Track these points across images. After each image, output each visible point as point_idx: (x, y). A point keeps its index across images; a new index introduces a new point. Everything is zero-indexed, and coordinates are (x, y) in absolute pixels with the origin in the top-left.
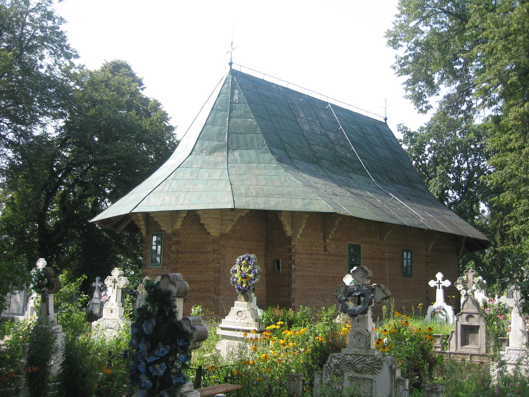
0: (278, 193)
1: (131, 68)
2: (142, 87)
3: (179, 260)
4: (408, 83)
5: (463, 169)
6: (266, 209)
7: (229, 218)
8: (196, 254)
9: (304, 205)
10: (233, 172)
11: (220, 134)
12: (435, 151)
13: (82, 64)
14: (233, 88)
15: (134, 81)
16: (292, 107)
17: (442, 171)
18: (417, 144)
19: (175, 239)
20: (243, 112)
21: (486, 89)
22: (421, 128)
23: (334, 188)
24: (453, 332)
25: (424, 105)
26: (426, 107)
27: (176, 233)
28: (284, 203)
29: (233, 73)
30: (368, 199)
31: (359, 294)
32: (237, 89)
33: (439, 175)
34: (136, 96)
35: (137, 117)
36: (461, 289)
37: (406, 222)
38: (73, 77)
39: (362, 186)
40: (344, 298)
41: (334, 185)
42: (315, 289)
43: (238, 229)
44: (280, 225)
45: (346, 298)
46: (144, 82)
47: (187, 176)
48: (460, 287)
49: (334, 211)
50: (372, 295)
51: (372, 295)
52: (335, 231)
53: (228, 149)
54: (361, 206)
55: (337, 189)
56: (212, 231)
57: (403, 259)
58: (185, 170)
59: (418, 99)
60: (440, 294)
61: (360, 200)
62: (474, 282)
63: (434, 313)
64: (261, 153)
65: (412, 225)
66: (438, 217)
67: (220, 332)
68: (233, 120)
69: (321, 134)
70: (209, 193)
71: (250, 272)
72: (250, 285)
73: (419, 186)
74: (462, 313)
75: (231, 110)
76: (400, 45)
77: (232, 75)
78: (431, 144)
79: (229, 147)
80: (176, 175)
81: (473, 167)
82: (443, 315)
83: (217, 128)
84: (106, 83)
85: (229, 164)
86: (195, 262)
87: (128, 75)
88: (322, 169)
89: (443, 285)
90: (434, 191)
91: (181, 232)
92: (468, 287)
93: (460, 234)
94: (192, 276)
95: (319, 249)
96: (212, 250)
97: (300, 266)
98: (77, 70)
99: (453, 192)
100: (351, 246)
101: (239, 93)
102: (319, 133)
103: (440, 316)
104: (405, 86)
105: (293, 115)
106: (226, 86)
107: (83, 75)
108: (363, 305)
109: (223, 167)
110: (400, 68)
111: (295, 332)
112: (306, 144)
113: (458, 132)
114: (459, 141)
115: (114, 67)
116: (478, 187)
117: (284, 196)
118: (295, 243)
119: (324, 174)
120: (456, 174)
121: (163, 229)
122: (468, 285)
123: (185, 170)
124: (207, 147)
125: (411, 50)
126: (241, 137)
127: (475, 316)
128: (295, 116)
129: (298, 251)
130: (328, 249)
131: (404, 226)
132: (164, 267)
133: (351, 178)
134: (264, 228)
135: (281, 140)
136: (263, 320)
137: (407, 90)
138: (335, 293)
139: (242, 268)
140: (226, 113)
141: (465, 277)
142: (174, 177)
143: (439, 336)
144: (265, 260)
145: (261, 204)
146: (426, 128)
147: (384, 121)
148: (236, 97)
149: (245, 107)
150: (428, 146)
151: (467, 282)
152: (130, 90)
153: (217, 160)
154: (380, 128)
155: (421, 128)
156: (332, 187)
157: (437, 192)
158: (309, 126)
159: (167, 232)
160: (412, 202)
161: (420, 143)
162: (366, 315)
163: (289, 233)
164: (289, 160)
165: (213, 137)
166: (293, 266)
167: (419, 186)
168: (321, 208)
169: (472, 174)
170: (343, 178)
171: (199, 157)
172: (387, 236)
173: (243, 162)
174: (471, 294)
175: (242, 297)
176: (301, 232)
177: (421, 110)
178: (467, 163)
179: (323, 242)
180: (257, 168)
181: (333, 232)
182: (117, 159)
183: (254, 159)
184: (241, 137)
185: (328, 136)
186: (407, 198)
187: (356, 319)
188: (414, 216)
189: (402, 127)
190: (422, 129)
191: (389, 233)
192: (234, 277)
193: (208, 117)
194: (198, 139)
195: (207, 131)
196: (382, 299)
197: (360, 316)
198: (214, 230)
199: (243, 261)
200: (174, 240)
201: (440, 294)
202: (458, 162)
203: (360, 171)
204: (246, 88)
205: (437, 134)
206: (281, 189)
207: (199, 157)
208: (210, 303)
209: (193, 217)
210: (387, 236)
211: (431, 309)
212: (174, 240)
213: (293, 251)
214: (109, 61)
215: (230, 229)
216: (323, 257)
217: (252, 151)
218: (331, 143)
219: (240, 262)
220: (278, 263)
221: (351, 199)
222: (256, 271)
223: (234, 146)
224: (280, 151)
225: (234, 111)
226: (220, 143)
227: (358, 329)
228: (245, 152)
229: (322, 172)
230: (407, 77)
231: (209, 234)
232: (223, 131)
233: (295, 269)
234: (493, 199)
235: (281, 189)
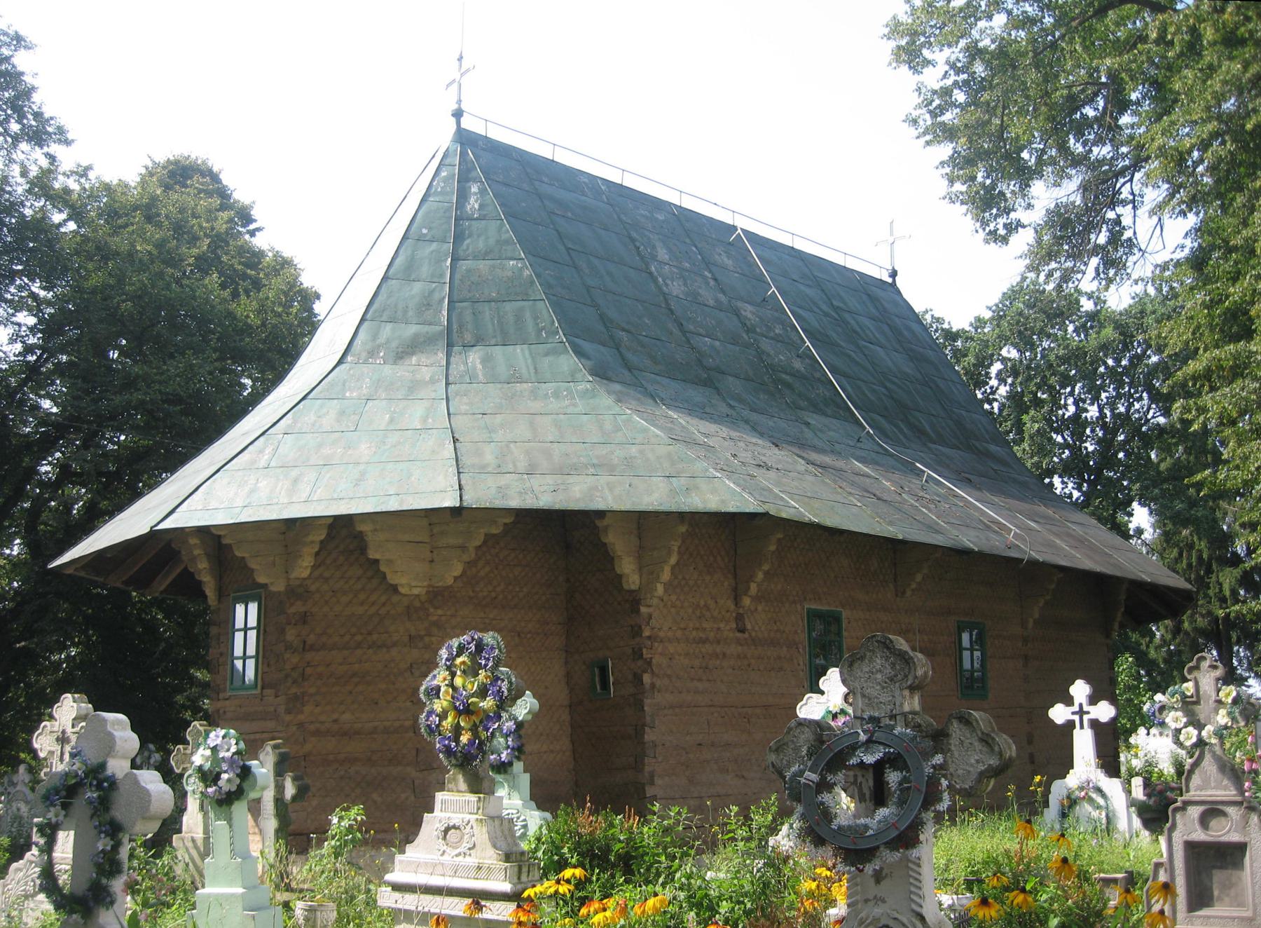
0: (595, 461)
1: (221, 176)
2: (252, 227)
3: (309, 670)
4: (953, 160)
5: (1086, 423)
6: (557, 507)
7: (452, 541)
8: (359, 652)
9: (673, 492)
10: (464, 408)
11: (427, 304)
12: (1016, 377)
13: (85, 164)
14: (464, 178)
15: (223, 207)
16: (634, 235)
17: (1037, 426)
18: (971, 359)
19: (297, 608)
20: (492, 241)
21: (1181, 154)
22: (978, 319)
23: (759, 449)
24: (1158, 866)
25: (1001, 221)
26: (1005, 225)
27: (296, 592)
28: (611, 490)
29: (464, 138)
30: (857, 479)
31: (879, 755)
32: (476, 180)
33: (1031, 437)
34: (227, 244)
35: (226, 294)
36: (1180, 725)
37: (969, 540)
38: (61, 199)
39: (837, 447)
40: (814, 777)
41: (760, 442)
42: (713, 745)
43: (482, 573)
44: (606, 558)
45: (823, 778)
46: (255, 213)
47: (328, 422)
48: (1176, 720)
49: (760, 510)
50: (938, 759)
51: (938, 759)
52: (767, 573)
53: (450, 345)
54: (839, 498)
55: (769, 453)
56: (404, 581)
57: (961, 649)
58: (321, 407)
59: (986, 203)
60: (1084, 744)
61: (834, 481)
62: (1219, 702)
63: (1071, 802)
64: (547, 354)
66: (1054, 529)
67: (387, 899)
68: (464, 265)
69: (719, 307)
70: (390, 466)
71: (483, 692)
72: (483, 735)
73: (993, 448)
74: (1187, 804)
75: (459, 238)
76: (928, 62)
77: (462, 144)
78: (1004, 360)
79: (453, 340)
80: (295, 421)
81: (1114, 415)
82: (1099, 807)
83: (417, 288)
84: (149, 210)
85: (451, 387)
86: (354, 675)
87: (209, 194)
88: (724, 399)
89: (1092, 716)
91: (313, 588)
92: (1202, 717)
93: (1118, 574)
94: (347, 716)
95: (722, 625)
96: (406, 639)
97: (669, 677)
98: (72, 179)
99: (1063, 482)
100: (814, 615)
101: (482, 192)
102: (711, 303)
103: (1088, 807)
104: (947, 170)
105: (639, 254)
106: (444, 174)
107: (93, 196)
108: (901, 803)
109: (433, 395)
110: (929, 122)
111: (624, 910)
112: (676, 331)
113: (1071, 328)
114: (1078, 348)
115: (172, 174)
116: (1127, 466)
117: (611, 469)
118: (651, 610)
119: (730, 412)
120: (1072, 435)
121: (261, 579)
122: (1202, 711)
123: (321, 407)
124: (388, 341)
125: (958, 71)
126: (487, 311)
127: (1231, 810)
128: (642, 258)
129: (661, 634)
130: (749, 627)
131: (964, 553)
132: (268, 692)
133: (807, 424)
134: (553, 567)
135: (603, 318)
136: (536, 850)
137: (952, 182)
138: (772, 757)
139: (458, 681)
140: (445, 246)
141: (1189, 687)
142: (289, 426)
143: (1115, 881)
144: (566, 663)
145: (543, 494)
146: (992, 319)
147: (890, 280)
148: (473, 204)
150: (996, 367)
151: (1197, 703)
152: (213, 229)
153: (418, 377)
154: (878, 300)
155: (978, 319)
158: (685, 284)
159: (273, 589)
160: (980, 489)
161: (977, 357)
162: (914, 853)
163: (633, 580)
164: (626, 372)
165: (405, 311)
166: (647, 678)
167: (993, 448)
168: (723, 502)
169: (1111, 431)
170: (782, 424)
171: (365, 370)
172: (914, 586)
173: (493, 379)
174: (1214, 741)
175: (460, 778)
176: (666, 575)
177: (994, 237)
178: (1099, 406)
179: (733, 607)
180: (534, 395)
181: (760, 576)
182: (164, 402)
183: (524, 371)
184: (487, 311)
185: (737, 313)
186: (964, 479)
187: (869, 869)
188: (988, 526)
190: (979, 322)
191: (919, 578)
192: (431, 713)
193: (393, 259)
194: (363, 320)
195: (389, 297)
196: (981, 774)
197: (891, 856)
198: (409, 578)
199: (458, 655)
200: (292, 610)
201: (1084, 744)
202: (1076, 403)
203: (833, 407)
204: (501, 178)
205: (1020, 332)
206: (602, 451)
207: (365, 369)
208: (403, 796)
209: (343, 535)
210: (914, 586)
211: (1059, 789)
212: (292, 610)
213: (647, 633)
214: (161, 158)
215: (457, 573)
216: (734, 649)
217: (518, 349)
218: (748, 331)
219: (451, 659)
220: (603, 671)
221: (811, 478)
222: (504, 689)
223: (468, 337)
224: (602, 349)
225: (467, 242)
226: (426, 328)
227: (877, 911)
228: (498, 351)
229: (724, 409)
230: (945, 150)
231: (394, 589)
232: (437, 296)
233: (653, 686)
234: (1199, 477)
235: (602, 451)
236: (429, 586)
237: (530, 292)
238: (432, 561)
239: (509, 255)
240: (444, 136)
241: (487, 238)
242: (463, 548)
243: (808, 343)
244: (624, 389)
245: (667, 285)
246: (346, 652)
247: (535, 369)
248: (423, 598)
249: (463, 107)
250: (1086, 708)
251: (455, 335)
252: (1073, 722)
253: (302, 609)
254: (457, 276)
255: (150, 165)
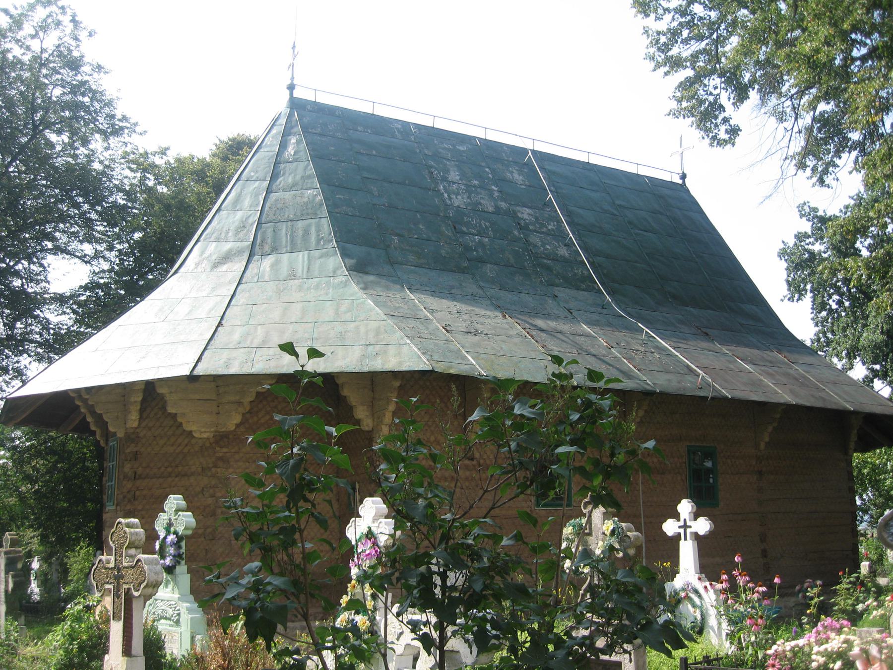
3: (138, 493)
7: (232, 398)
8: (170, 479)
11: (243, 226)
14: (286, 134)
20: (298, 177)
29: (296, 104)
43: (263, 421)
56: (194, 428)
60: (687, 552)
64: (321, 257)
65: (671, 390)
68: (273, 197)
75: (274, 176)
89: (693, 530)
90: (877, 326)
91: (141, 435)
96: (200, 470)
101: (298, 142)
102: (491, 209)
126: (283, 229)
146: (855, 205)
147: (680, 182)
148: (291, 150)
149: (305, 169)
156: (491, 320)
157: (882, 327)
158: (469, 197)
177: (722, 143)
180: (300, 288)
183: (300, 271)
185: (514, 215)
189: (807, 210)
195: (218, 223)
198: (199, 425)
201: (687, 552)
203: (582, 283)
212: (128, 451)
223: (267, 248)
225: (281, 179)
226: (239, 244)
229: (472, 288)
232: (251, 220)
236: (216, 431)
237: (318, 212)
238: (218, 413)
239: (309, 186)
240: (281, 105)
241: (295, 175)
242: (239, 403)
243: (571, 235)
244: (378, 280)
245: (450, 199)
246: (161, 480)
247: (308, 269)
248: (212, 440)
249: (295, 82)
250: (688, 523)
251: (257, 247)
252: (679, 534)
253: (135, 450)
254: (268, 205)
255: (218, 143)
